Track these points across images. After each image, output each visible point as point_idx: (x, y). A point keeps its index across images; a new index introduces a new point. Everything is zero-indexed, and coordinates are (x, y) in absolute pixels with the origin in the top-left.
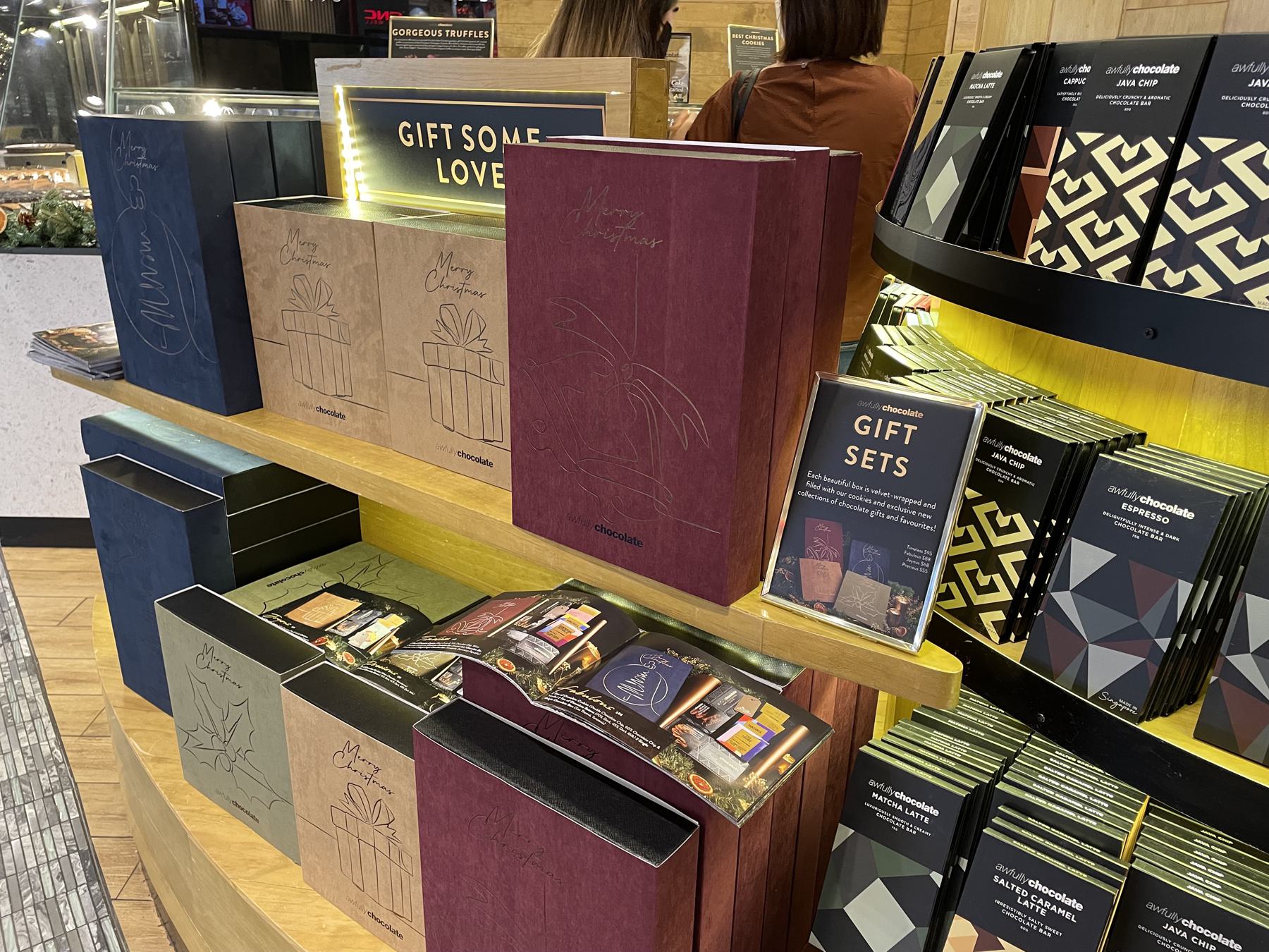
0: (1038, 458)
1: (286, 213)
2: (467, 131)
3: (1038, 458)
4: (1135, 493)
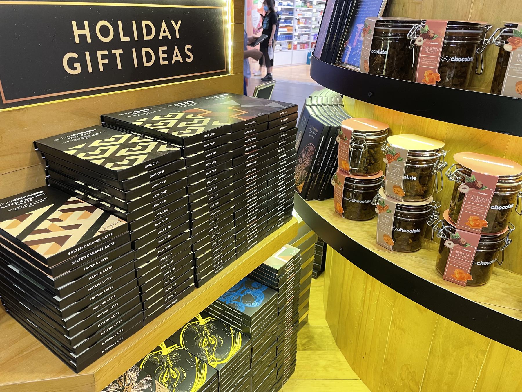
1: (438, 52)
2: (188, 49)
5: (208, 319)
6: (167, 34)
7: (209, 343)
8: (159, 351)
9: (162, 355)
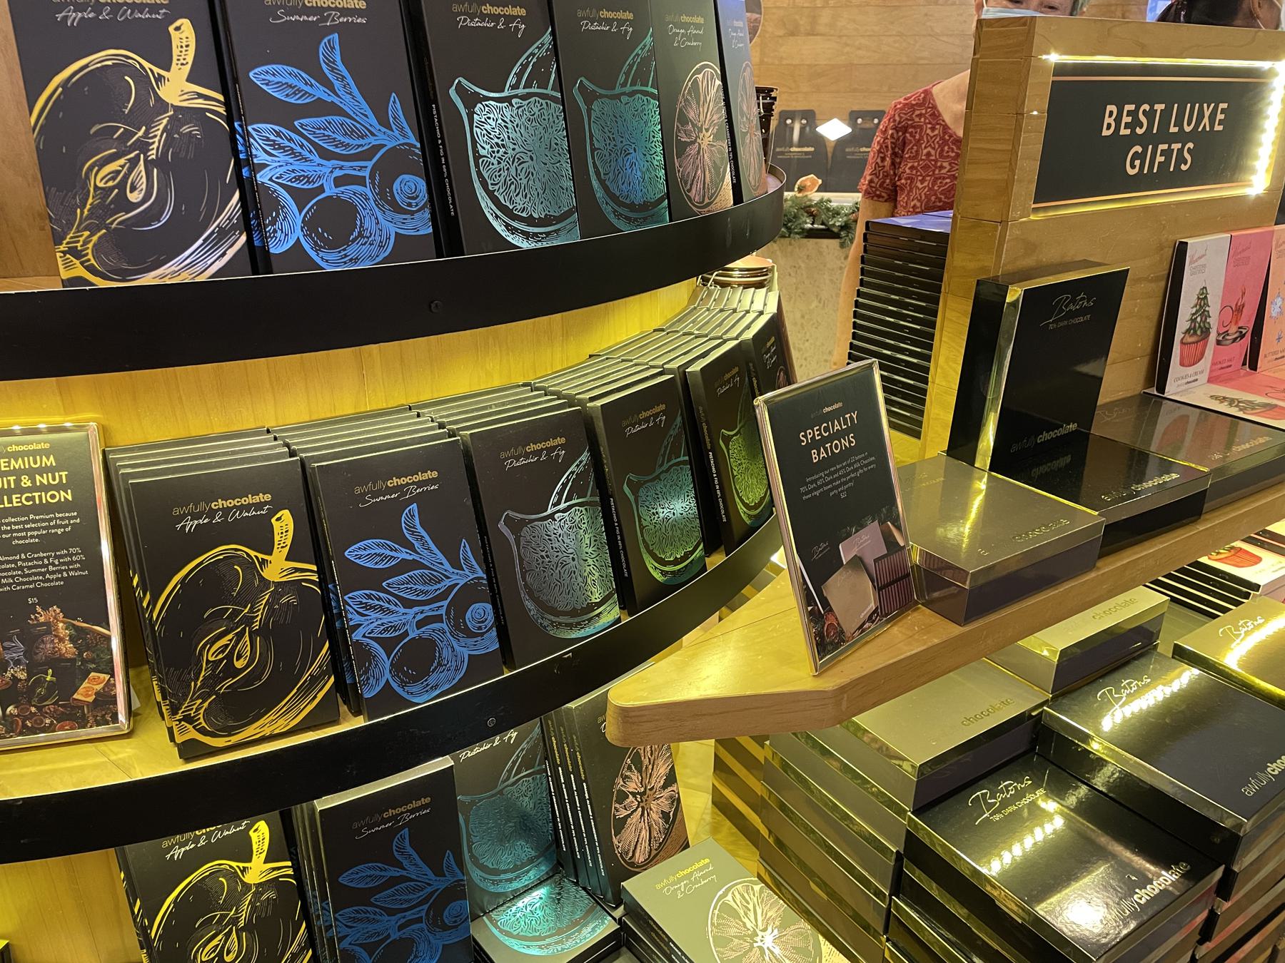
0: (264, 494)
3: (264, 494)
4: (380, 482)
5: (200, 96)
6: (825, 455)
7: (122, 186)
8: (156, 70)
9: (155, 93)
